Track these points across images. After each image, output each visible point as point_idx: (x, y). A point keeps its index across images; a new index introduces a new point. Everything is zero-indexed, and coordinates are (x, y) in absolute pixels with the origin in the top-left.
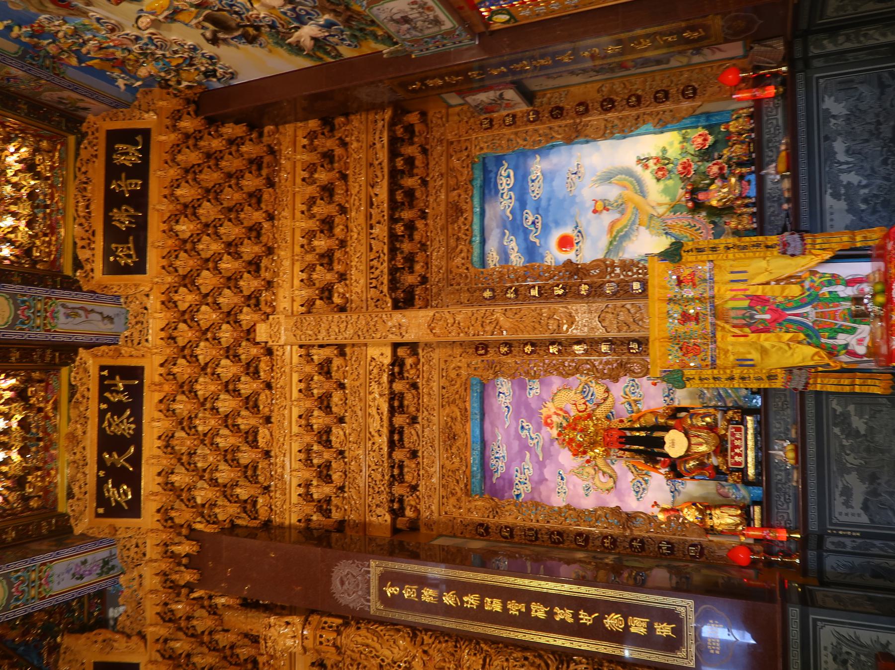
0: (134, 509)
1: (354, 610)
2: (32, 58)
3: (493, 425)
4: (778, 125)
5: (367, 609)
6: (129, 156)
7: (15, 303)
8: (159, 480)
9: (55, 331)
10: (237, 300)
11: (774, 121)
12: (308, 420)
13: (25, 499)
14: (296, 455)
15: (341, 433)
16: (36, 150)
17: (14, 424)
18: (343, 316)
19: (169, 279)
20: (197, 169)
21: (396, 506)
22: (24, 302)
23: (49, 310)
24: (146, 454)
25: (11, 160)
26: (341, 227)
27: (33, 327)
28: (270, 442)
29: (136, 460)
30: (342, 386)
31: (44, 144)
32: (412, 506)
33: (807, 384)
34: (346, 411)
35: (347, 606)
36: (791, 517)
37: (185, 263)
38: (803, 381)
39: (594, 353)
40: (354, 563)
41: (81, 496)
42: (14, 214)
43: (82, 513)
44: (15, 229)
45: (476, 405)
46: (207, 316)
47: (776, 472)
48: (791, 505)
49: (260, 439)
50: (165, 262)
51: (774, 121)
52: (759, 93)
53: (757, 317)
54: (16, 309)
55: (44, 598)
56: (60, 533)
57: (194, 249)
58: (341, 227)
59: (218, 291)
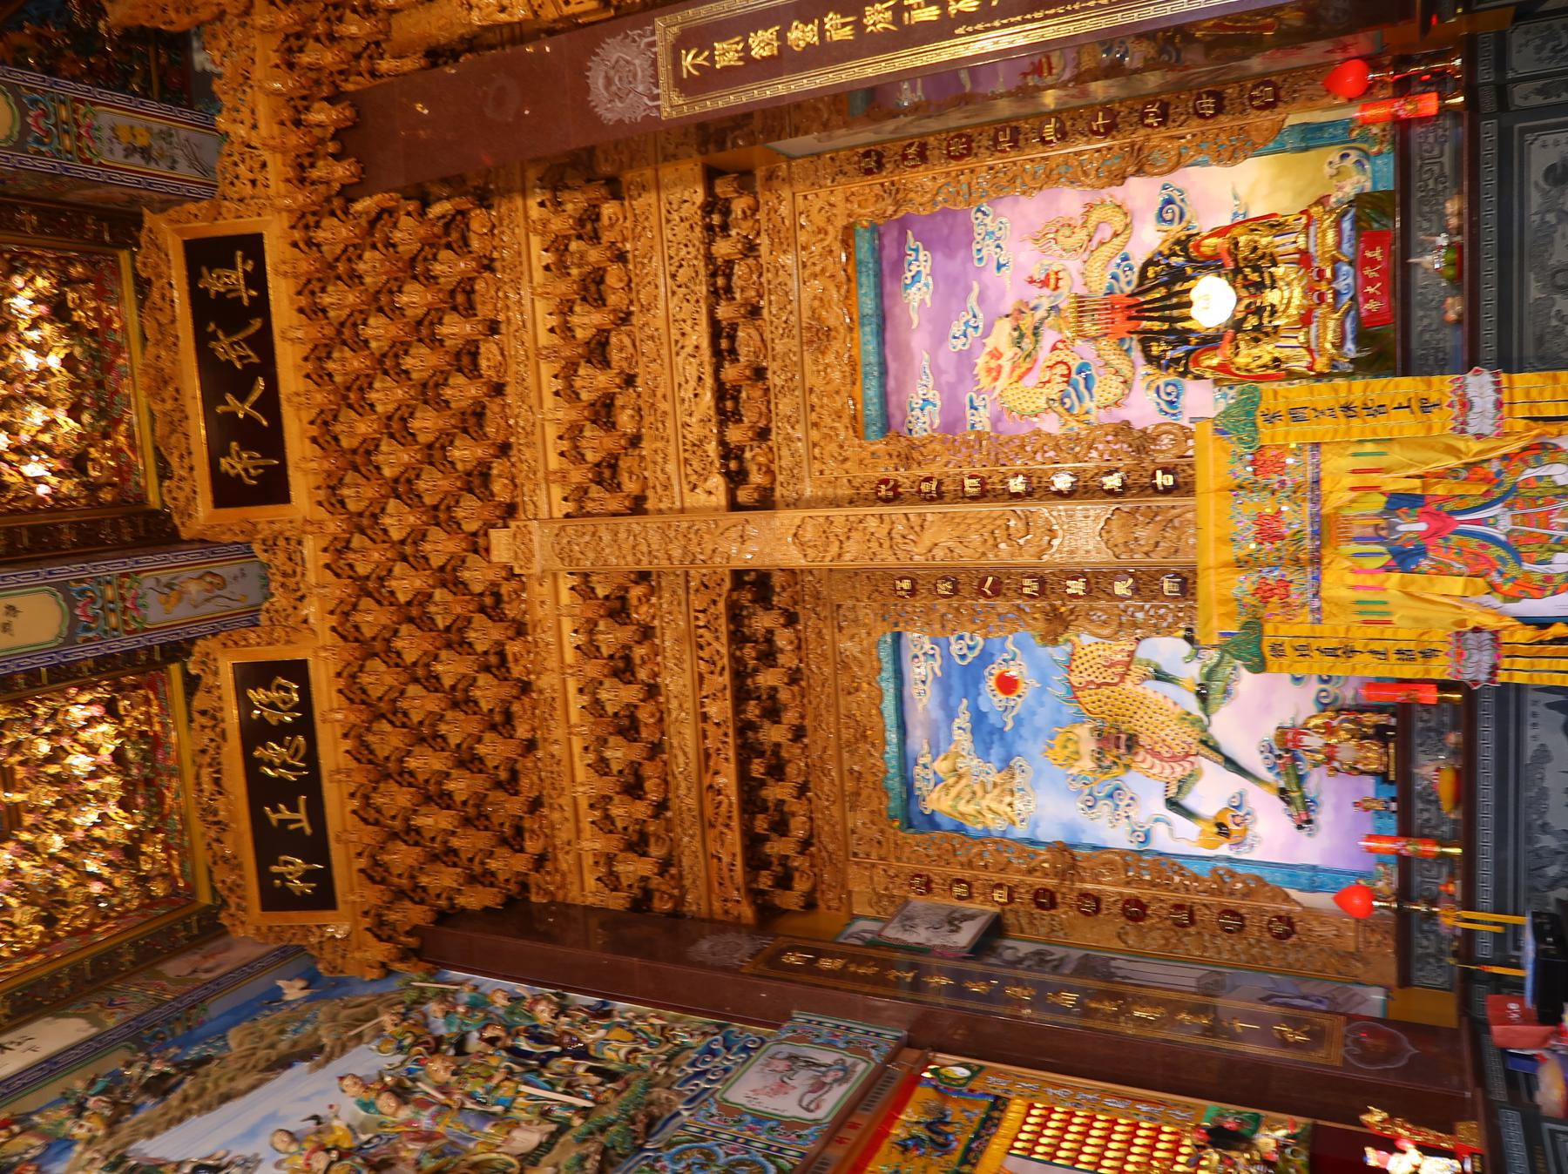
0: (274, 488)
1: (633, 124)
2: (39, 141)
3: (901, 386)
4: (1442, 175)
5: (654, 114)
6: (230, 280)
7: (19, 102)
8: (348, 744)
9: (100, 164)
10: (473, 726)
11: (1436, 168)
12: (595, 693)
13: (92, 488)
14: (539, 258)
15: (627, 341)
16: (65, 281)
17: (54, 361)
18: (644, 566)
19: (319, 398)
20: (358, 318)
21: (733, 465)
22: (82, 592)
23: (128, 595)
24: (278, 324)
25: (21, 302)
26: (630, 412)
27: (59, 151)
28: (502, 367)
29: (270, 403)
30: (621, 257)
31: (77, 271)
32: (760, 466)
33: (1495, 668)
34: (631, 302)
35: (620, 122)
36: (1447, 170)
37: (357, 495)
38: (1486, 667)
39: (1102, 595)
40: (627, 36)
41: (183, 473)
42: (42, 400)
43: (191, 500)
44: (50, 425)
45: (871, 347)
46: (398, 520)
47: (1421, 313)
48: (1447, 147)
49: (483, 363)
50: (303, 301)
51: (1436, 168)
52: (1405, 109)
53: (1401, 528)
54: (24, 113)
55: (89, 161)
56: (154, 532)
57: (389, 650)
58: (630, 412)
59: (394, 287)
